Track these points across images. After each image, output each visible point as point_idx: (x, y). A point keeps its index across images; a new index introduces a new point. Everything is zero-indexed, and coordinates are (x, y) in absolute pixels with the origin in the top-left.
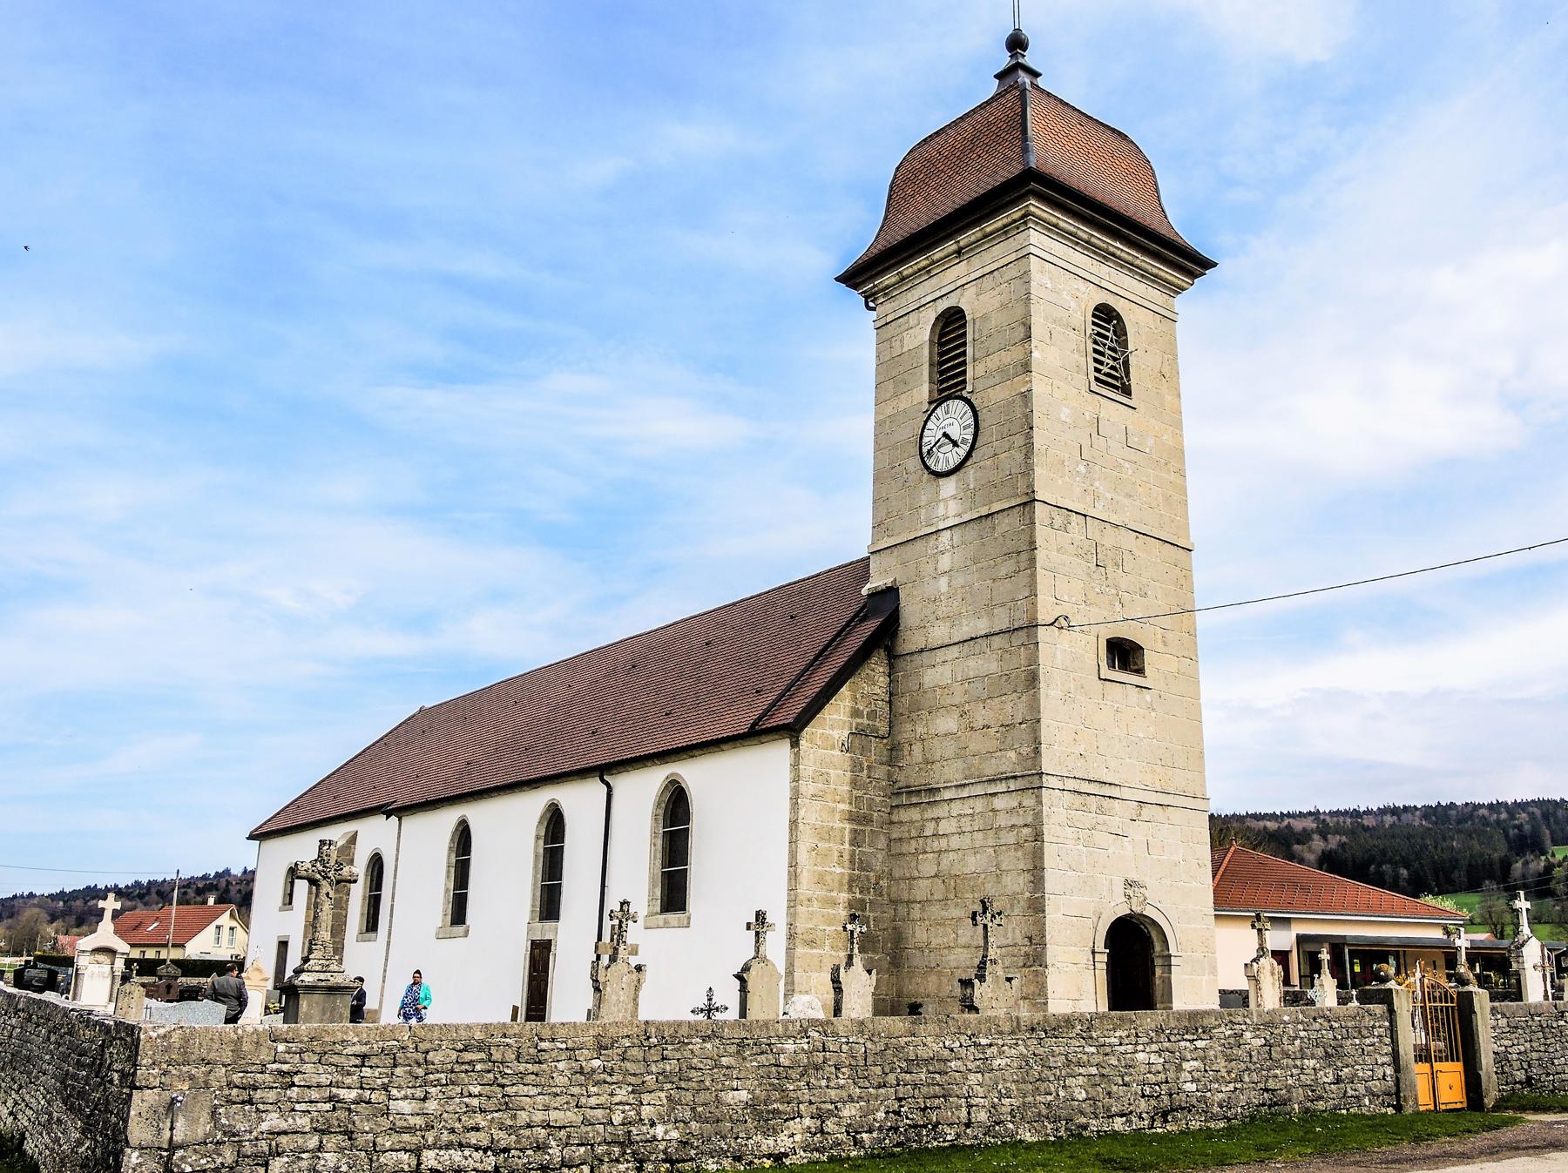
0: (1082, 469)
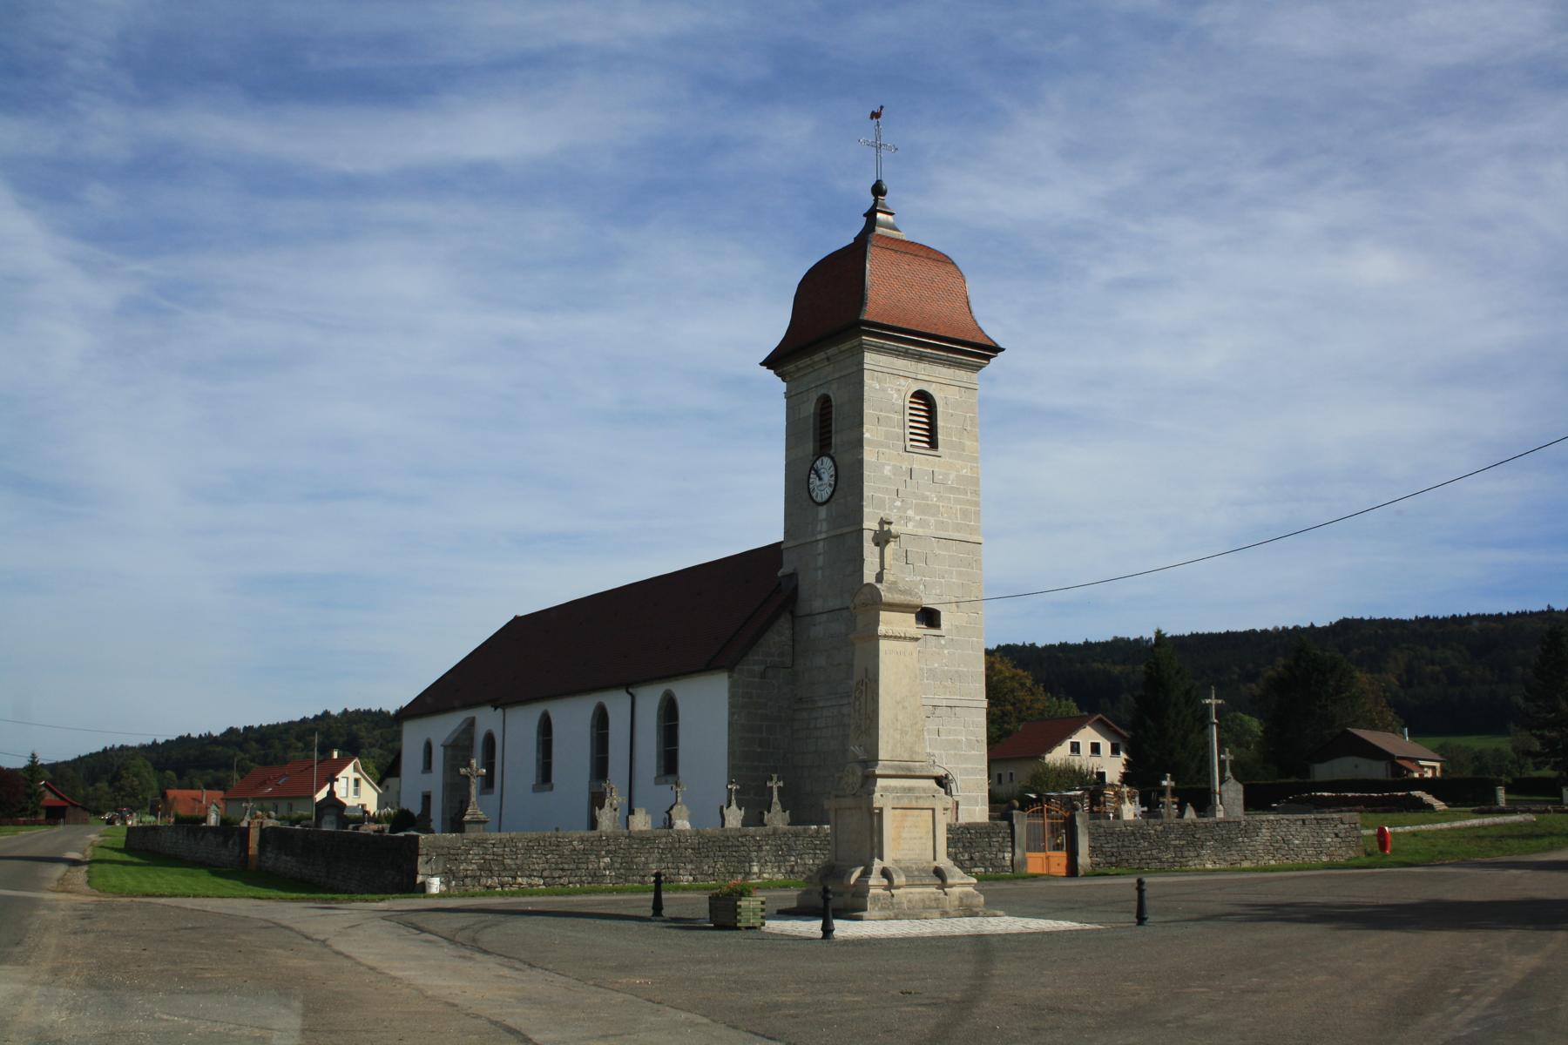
0: (898, 503)
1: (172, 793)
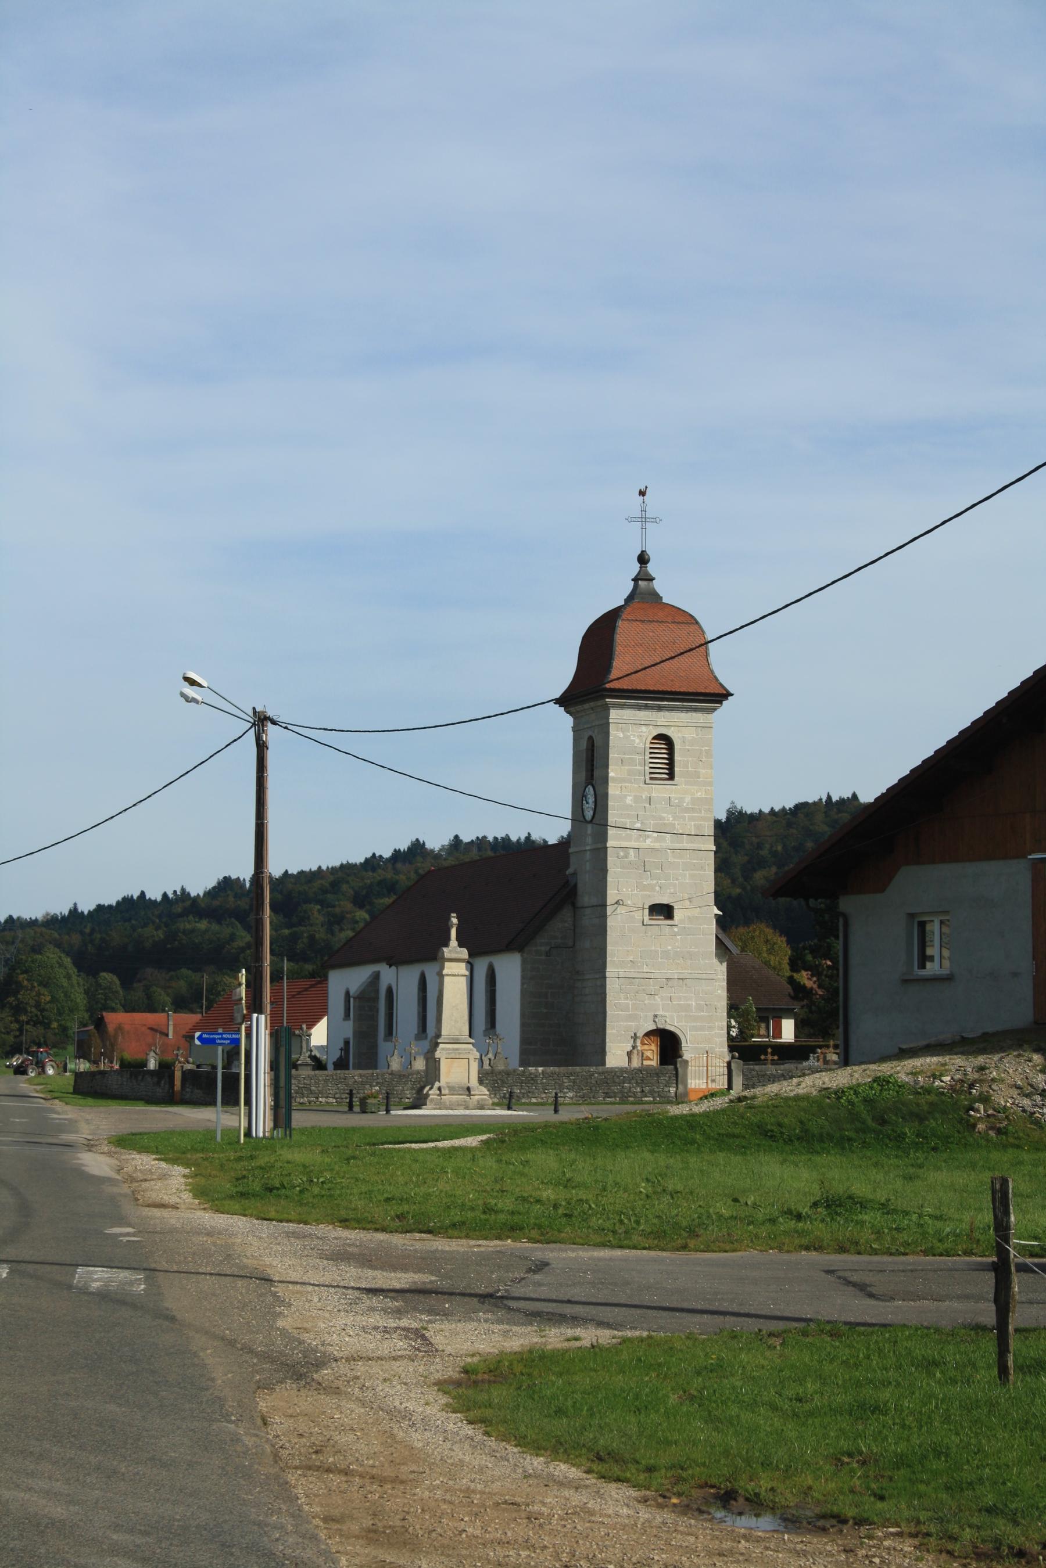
1: (114, 1019)
